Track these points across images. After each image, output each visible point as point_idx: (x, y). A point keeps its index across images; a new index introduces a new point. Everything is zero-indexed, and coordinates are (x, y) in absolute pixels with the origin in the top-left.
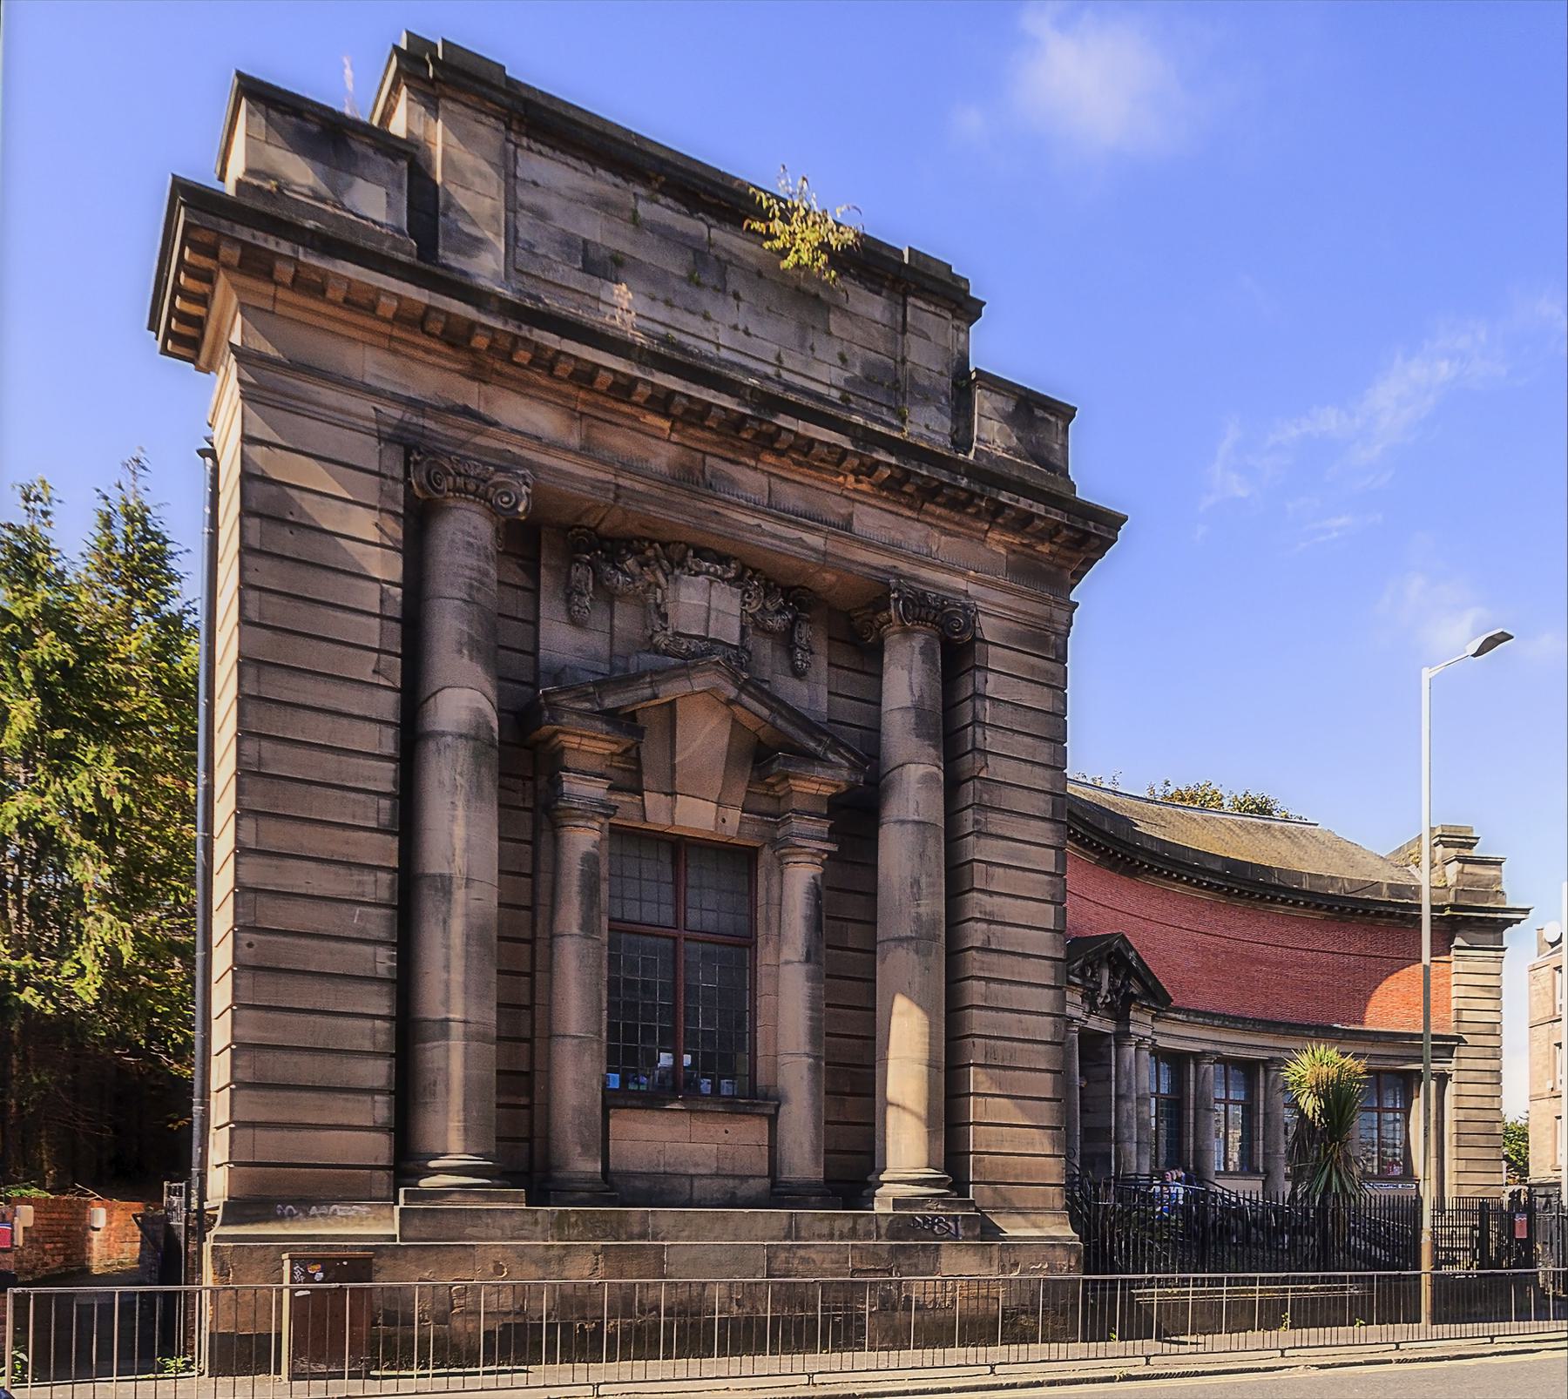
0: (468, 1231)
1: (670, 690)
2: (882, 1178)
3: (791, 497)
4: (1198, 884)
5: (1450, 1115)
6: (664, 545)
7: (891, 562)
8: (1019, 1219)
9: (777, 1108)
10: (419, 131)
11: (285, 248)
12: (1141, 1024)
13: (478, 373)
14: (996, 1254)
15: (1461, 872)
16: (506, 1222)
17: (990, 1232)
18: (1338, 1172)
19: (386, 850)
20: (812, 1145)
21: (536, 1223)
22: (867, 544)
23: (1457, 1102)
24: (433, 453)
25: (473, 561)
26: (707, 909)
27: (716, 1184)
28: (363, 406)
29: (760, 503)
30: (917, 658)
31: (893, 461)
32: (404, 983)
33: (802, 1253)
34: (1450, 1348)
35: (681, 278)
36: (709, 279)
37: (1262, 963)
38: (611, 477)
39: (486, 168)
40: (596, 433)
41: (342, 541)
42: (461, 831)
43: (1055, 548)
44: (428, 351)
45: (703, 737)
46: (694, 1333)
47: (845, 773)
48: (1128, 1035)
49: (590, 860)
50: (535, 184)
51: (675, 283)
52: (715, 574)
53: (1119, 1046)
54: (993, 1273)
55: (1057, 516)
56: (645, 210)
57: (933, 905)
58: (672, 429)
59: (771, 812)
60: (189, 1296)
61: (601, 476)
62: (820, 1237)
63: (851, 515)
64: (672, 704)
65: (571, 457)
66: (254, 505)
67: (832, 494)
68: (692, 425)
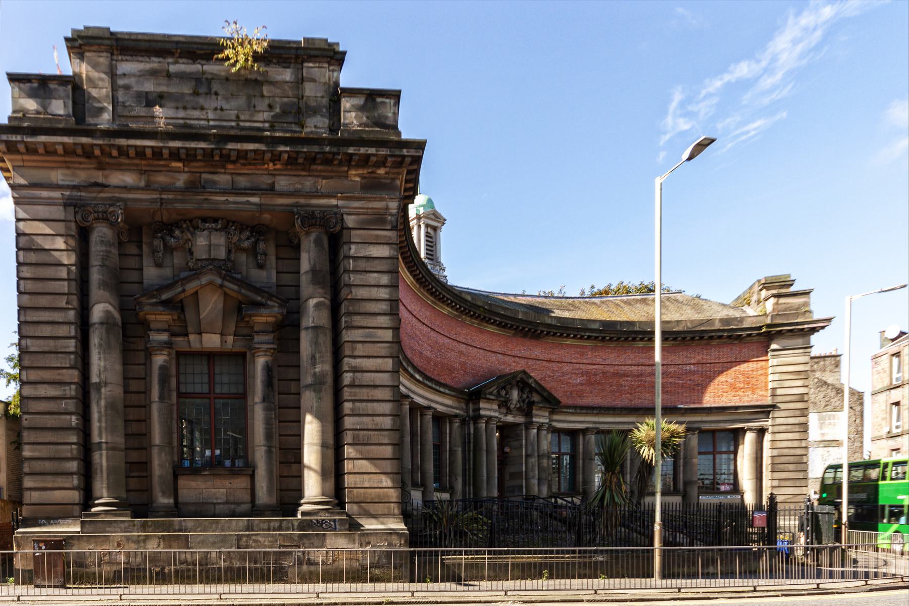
0: (107, 529)
1: (191, 287)
2: (302, 501)
3: (243, 182)
4: (582, 337)
5: (767, 453)
6: (191, 221)
7: (296, 200)
8: (373, 521)
9: (254, 471)
10: (77, 70)
11: (19, 138)
12: (541, 417)
13: (101, 167)
14: (357, 537)
15: (777, 304)
16: (122, 525)
17: (354, 526)
18: (611, 490)
19: (74, 375)
20: (267, 487)
21: (134, 525)
22: (282, 194)
23: (772, 445)
24: (83, 206)
25: (103, 248)
26: (225, 381)
27: (226, 507)
28: (56, 194)
30: (312, 245)
31: (288, 149)
32: (85, 430)
33: (254, 537)
34: (649, 594)
35: (191, 94)
36: (203, 90)
37: (628, 376)
38: (158, 196)
39: (103, 76)
40: (152, 178)
41: (53, 253)
42: (103, 365)
43: (388, 169)
44: (80, 163)
45: (211, 305)
46: (210, 575)
47: (276, 309)
48: (532, 423)
49: (164, 369)
50: (124, 75)
51: (187, 98)
52: (212, 228)
53: (527, 429)
54: (356, 547)
55: (383, 152)
56: (173, 68)
57: (324, 367)
58: (184, 166)
59: (246, 333)
60: (653, 550)
61: (154, 196)
62: (263, 530)
63: (274, 183)
64: (196, 293)
65: (140, 192)
66: (21, 245)
68: (192, 161)
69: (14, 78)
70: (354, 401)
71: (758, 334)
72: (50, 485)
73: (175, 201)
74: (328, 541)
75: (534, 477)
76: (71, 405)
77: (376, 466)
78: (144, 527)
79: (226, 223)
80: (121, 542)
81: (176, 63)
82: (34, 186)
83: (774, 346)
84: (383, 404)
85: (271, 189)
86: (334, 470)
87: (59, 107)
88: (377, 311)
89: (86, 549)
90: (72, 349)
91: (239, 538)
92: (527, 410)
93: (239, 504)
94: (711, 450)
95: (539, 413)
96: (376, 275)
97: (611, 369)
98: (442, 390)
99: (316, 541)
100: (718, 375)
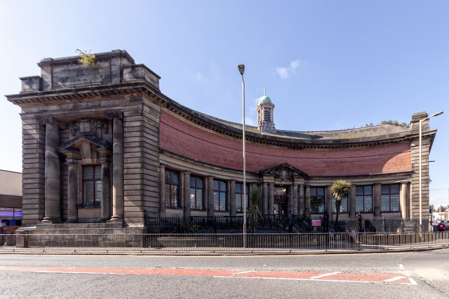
3: (90, 104)
4: (322, 147)
8: (133, 224)
13: (46, 105)
15: (413, 125)
22: (102, 107)
28: (33, 115)
29: (87, 107)
36: (80, 74)
45: (86, 148)
47: (103, 148)
53: (293, 187)
67: (96, 101)
69: (22, 79)
70: (127, 180)
71: (404, 140)
72: (30, 213)
73: (69, 113)
74: (114, 232)
75: (295, 206)
76: (37, 186)
77: (135, 204)
78: (55, 227)
79: (89, 119)
80: (47, 231)
81: (72, 66)
82: (27, 113)
83: (412, 145)
84: (137, 180)
85: (99, 106)
86: (121, 205)
87: (35, 86)
88: (135, 146)
89: (38, 234)
90: (38, 167)
91: (85, 230)
92: (292, 178)
93: (97, 218)
94: (388, 192)
95: (298, 180)
96: (135, 133)
97: (338, 160)
98: (239, 172)
99: (110, 231)
100: (388, 160)
